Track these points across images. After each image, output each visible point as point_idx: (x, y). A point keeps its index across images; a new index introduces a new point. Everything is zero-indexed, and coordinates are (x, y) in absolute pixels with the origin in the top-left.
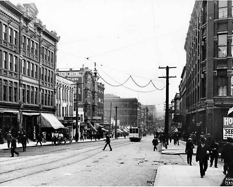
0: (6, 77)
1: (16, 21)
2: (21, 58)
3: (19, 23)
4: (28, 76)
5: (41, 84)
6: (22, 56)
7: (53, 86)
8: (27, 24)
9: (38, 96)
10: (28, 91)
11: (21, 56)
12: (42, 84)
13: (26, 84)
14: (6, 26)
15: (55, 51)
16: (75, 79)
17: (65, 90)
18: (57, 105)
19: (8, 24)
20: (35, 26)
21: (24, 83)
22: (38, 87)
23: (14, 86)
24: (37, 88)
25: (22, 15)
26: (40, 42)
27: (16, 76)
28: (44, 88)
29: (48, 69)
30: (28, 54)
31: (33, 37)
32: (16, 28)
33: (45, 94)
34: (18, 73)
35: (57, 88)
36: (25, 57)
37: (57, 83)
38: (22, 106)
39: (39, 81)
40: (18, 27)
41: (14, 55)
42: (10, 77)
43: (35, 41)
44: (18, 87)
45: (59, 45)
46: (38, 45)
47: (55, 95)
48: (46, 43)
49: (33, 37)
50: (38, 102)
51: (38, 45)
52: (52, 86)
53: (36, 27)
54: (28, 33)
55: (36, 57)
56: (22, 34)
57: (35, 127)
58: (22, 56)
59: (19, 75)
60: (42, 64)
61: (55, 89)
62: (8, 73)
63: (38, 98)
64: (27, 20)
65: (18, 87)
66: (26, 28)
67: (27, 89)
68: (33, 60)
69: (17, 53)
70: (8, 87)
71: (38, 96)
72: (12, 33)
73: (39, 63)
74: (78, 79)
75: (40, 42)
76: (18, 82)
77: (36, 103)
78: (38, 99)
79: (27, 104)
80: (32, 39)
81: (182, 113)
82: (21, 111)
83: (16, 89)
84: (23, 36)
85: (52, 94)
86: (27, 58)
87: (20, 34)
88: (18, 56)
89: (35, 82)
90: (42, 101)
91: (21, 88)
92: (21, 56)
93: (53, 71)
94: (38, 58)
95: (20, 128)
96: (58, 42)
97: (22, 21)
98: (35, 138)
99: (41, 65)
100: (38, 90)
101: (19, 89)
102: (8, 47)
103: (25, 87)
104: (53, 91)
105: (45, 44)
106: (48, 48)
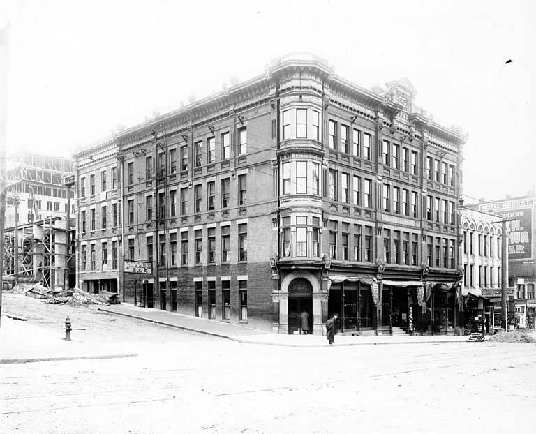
0: (347, 217)
1: (368, 116)
2: (378, 182)
3: (375, 119)
4: (406, 216)
5: (425, 226)
6: (381, 178)
7: (456, 229)
8: (391, 120)
9: (419, 250)
10: (406, 243)
11: (424, 190)
12: (430, 227)
13: (392, 228)
14: (398, 146)
15: (459, 162)
16: (517, 214)
17: (485, 236)
18: (465, 265)
19: (352, 123)
20: (410, 120)
21: (385, 226)
22: (419, 232)
23: (412, 239)
24: (453, 241)
25: (380, 103)
26: (376, 128)
27: (369, 216)
28: (434, 235)
29: (442, 197)
30: (436, 184)
31: (406, 140)
32: (370, 129)
33: (437, 246)
34: (374, 210)
35: (465, 232)
36: (388, 178)
37: (466, 224)
38: (382, 269)
39: (421, 221)
40: (369, 125)
41: (364, 177)
42: (333, 213)
43: (411, 148)
44: (374, 234)
45: (466, 150)
46: (419, 155)
47: (460, 248)
48: (401, 134)
49: (406, 140)
50: (420, 260)
51: (419, 155)
52: (453, 229)
53: (412, 122)
54: (414, 141)
55: (413, 178)
56: (381, 137)
57: (411, 308)
58: (381, 178)
59: (376, 212)
60: (329, 161)
61: (459, 236)
62: (442, 227)
63: (420, 253)
64: (391, 112)
65: (374, 234)
66: (390, 126)
67: (394, 236)
68: (405, 183)
69: (372, 174)
70: (352, 236)
71: (419, 250)
72: (446, 171)
73: (421, 188)
74: (522, 214)
75: (423, 147)
76: (373, 225)
77: (452, 267)
78: (420, 256)
79: (435, 268)
80: (354, 126)
81: (198, 268)
82: (380, 278)
83: (415, 244)
84: (428, 157)
85: (454, 244)
86: (393, 180)
87: (376, 137)
88: (418, 191)
89: (412, 223)
90: (430, 258)
91: (378, 236)
92: (379, 179)
93: (418, 191)
94: (419, 179)
95: (378, 310)
96: (464, 143)
97: (380, 115)
98: (412, 329)
99: (425, 191)
100: (456, 244)
101: (376, 238)
102: (411, 181)
103: (432, 241)
104: (455, 238)
105: (436, 150)
106: (442, 157)
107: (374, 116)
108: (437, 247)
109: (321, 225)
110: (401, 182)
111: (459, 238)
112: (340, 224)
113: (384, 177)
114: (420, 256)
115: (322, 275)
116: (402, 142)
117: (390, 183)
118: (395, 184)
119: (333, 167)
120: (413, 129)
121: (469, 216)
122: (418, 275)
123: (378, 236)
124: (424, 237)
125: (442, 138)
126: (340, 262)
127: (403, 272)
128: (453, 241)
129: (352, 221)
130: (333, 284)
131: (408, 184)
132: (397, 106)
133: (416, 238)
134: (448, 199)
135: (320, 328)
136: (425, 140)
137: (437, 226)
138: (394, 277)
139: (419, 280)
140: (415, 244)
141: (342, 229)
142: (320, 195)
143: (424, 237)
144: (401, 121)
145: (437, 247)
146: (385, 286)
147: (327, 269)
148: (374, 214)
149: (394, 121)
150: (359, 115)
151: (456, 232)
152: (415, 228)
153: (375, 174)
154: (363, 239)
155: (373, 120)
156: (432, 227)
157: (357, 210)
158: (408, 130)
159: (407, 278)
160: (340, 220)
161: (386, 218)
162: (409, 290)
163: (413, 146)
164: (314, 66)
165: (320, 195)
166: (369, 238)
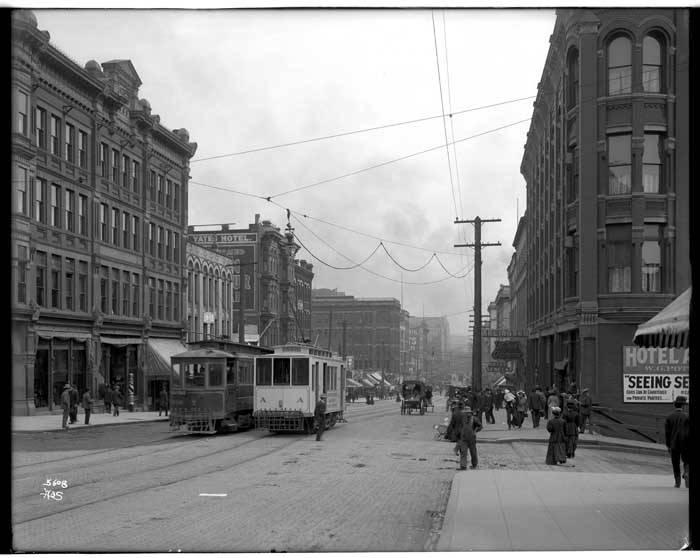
0: (57, 248)
5: (148, 264)
18: (189, 317)
19: (64, 114)
22: (140, 272)
26: (94, 126)
28: (157, 276)
34: (89, 238)
40: (87, 121)
43: (132, 157)
44: (89, 273)
45: (195, 166)
52: (176, 269)
53: (135, 121)
54: (115, 135)
56: (100, 139)
59: (92, 242)
61: (183, 279)
62: (64, 238)
64: (112, 105)
65: (89, 273)
67: (112, 278)
68: (126, 204)
73: (144, 212)
74: (243, 252)
76: (88, 259)
80: (67, 119)
85: (177, 290)
88: (89, 194)
91: (96, 276)
97: (99, 107)
100: (141, 281)
101: (93, 279)
103: (107, 274)
107: (92, 109)
108: (69, 275)
109: (28, 257)
110: (120, 202)
111: (183, 282)
112: (49, 255)
113: (103, 194)
114: (141, 303)
115: (27, 329)
116: (122, 147)
117: (108, 202)
118: (114, 204)
119: (42, 175)
120: (136, 131)
121: (194, 252)
122: (88, 324)
123: (96, 276)
124: (146, 278)
125: (60, 74)
126: (60, 312)
127: (124, 325)
128: (137, 275)
129: (64, 254)
130: (42, 340)
131: (130, 206)
132: (119, 98)
133: (85, 269)
134: (130, 211)
135: (24, 406)
136: (149, 147)
137: (55, 234)
138: (112, 332)
139: (138, 337)
140: (137, 288)
141: (52, 264)
142: (28, 215)
143: (146, 278)
144: (122, 117)
145: (69, 275)
146: (105, 345)
147: (34, 322)
148: (89, 244)
149: (115, 117)
150: (42, 84)
151: (89, 247)
152: (136, 266)
153: (92, 188)
154: (157, 293)
155: (89, 113)
156: (45, 236)
157: (70, 238)
158: (128, 130)
159: (127, 333)
160: (50, 250)
161: (104, 251)
162: (128, 349)
163: (134, 154)
164: (23, 29)
165: (28, 215)
166: (83, 278)
